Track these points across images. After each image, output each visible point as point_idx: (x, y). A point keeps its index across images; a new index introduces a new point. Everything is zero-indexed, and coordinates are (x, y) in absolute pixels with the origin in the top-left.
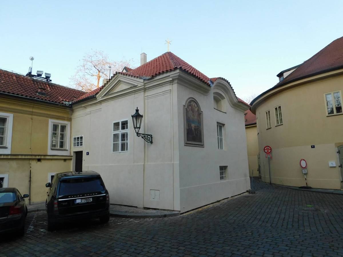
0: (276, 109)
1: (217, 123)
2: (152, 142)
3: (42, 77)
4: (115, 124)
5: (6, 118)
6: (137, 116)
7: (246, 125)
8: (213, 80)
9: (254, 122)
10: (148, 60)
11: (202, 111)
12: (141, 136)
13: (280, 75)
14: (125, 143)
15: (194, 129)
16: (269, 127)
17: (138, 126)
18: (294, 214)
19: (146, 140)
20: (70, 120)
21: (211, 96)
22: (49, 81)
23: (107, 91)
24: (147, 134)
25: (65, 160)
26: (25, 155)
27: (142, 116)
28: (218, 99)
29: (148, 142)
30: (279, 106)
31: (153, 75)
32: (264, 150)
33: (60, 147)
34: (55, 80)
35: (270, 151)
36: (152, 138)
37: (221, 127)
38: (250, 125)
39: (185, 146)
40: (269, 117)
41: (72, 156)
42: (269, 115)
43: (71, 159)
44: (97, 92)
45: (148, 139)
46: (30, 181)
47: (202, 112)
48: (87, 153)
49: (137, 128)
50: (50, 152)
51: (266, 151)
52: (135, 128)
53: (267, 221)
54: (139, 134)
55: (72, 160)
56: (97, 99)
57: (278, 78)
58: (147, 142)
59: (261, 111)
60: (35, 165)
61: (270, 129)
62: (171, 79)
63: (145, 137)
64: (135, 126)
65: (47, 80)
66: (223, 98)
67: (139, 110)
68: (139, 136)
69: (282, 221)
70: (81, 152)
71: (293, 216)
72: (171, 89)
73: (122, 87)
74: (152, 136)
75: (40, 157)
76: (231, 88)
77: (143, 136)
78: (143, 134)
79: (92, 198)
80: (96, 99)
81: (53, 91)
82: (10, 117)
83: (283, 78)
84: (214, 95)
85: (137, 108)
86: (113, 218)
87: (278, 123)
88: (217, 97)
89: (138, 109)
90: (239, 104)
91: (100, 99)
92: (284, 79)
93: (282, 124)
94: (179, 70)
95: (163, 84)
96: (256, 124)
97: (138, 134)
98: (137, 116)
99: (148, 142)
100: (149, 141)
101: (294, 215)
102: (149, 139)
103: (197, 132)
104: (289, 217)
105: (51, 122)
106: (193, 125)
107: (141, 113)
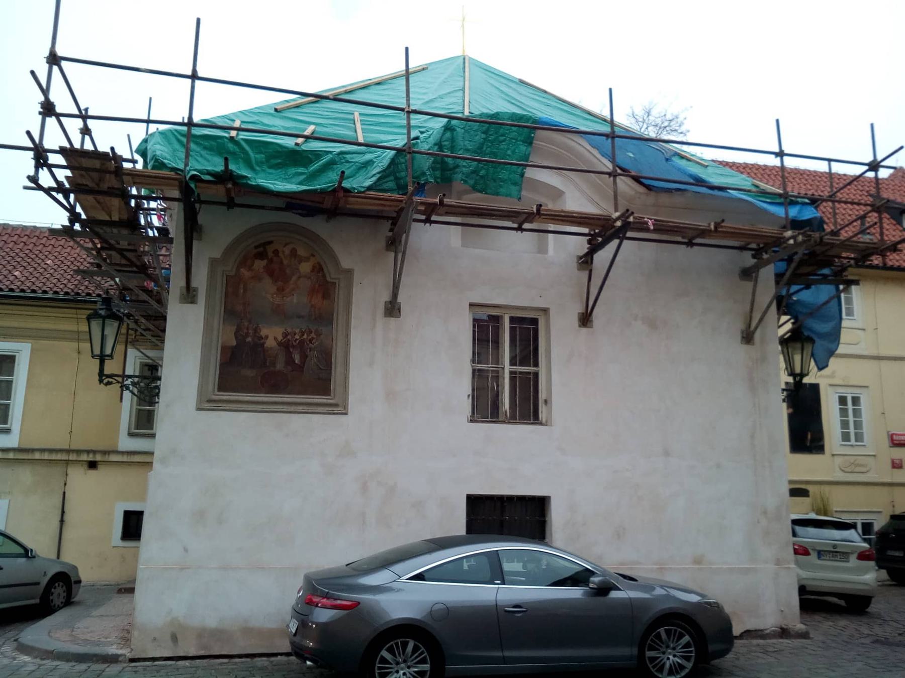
5: (15, 356)
12: (118, 382)
23: (372, 127)
26: (51, 451)
33: (856, 441)
46: (62, 521)
60: (79, 478)
75: (91, 455)
82: (23, 351)
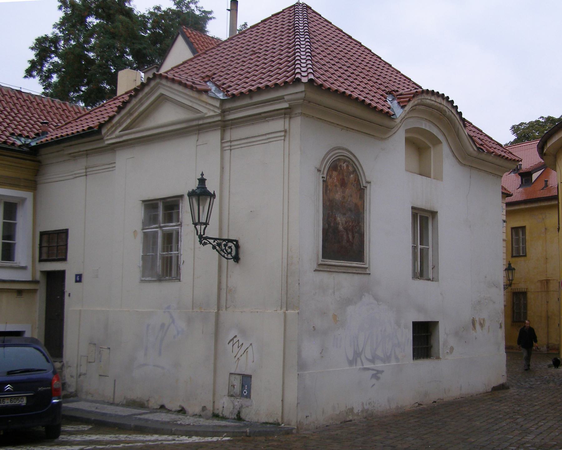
2: (237, 259)
4: (150, 205)
6: (201, 193)
11: (368, 180)
12: (210, 243)
14: (173, 255)
15: (344, 228)
17: (203, 220)
19: (223, 254)
20: (32, 185)
21: (399, 139)
24: (226, 238)
25: (20, 292)
27: (213, 196)
28: (419, 146)
36: (237, 247)
37: (427, 218)
39: (315, 271)
43: (35, 291)
45: (230, 250)
47: (369, 183)
48: (76, 275)
49: (202, 224)
52: (195, 224)
54: (206, 238)
55: (38, 292)
56: (105, 138)
61: (367, 276)
62: (286, 105)
63: (219, 245)
64: (197, 221)
66: (436, 142)
67: (206, 180)
68: (205, 244)
70: (61, 274)
72: (287, 127)
73: (167, 116)
77: (215, 243)
78: (215, 239)
79: (163, 202)
80: (102, 139)
84: (409, 135)
85: (202, 175)
89: (204, 177)
91: (111, 139)
95: (268, 114)
97: (203, 239)
98: (201, 193)
100: (229, 256)
102: (229, 250)
103: (350, 237)
106: (341, 219)
107: (211, 187)
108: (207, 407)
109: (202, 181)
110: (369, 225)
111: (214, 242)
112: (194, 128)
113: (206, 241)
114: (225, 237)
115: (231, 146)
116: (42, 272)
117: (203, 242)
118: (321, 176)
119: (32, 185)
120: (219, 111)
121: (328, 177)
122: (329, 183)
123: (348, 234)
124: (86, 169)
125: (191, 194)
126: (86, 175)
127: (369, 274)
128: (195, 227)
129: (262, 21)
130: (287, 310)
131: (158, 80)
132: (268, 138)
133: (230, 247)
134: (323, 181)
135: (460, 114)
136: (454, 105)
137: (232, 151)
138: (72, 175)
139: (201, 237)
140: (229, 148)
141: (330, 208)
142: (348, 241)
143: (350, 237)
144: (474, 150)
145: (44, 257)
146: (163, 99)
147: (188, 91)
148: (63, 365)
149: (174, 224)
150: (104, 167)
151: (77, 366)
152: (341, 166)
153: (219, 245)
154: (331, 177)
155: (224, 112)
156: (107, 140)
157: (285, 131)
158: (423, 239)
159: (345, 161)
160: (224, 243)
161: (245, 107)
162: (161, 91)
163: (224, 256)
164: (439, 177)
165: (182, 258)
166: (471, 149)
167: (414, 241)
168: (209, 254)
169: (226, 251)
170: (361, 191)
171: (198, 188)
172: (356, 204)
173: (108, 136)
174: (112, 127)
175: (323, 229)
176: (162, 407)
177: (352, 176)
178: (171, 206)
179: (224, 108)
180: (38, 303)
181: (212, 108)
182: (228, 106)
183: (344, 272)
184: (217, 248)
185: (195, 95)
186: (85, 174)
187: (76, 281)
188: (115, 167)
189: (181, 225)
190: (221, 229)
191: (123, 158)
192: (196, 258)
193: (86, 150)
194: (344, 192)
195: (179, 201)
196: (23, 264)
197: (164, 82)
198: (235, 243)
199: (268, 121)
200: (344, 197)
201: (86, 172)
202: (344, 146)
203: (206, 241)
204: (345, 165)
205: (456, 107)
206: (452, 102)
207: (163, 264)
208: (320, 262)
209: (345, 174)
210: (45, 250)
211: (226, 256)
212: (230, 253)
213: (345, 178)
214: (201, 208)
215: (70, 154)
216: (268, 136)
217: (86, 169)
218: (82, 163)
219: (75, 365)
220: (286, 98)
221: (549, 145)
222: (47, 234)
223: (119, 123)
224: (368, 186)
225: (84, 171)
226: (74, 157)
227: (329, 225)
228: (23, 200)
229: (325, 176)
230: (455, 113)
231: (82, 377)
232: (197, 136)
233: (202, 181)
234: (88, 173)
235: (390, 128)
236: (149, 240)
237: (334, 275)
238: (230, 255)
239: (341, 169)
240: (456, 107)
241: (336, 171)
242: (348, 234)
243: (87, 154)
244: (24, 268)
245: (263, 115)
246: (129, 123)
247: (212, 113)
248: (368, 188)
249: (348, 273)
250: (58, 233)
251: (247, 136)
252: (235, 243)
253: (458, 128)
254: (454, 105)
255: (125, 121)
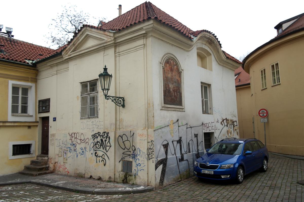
0: (273, 66)
1: (202, 83)
2: (123, 106)
3: (2, 31)
4: (84, 85)
7: (236, 87)
8: (196, 34)
9: (247, 83)
10: (124, 11)
11: (182, 69)
12: (111, 99)
13: (278, 27)
15: (173, 90)
16: (265, 88)
17: (106, 87)
18: (291, 189)
19: (117, 104)
22: (11, 37)
25: (29, 127)
29: (119, 106)
30: (276, 63)
31: (124, 27)
32: (259, 113)
34: (18, 36)
35: (265, 114)
36: (124, 100)
37: (206, 87)
38: (242, 87)
39: (161, 110)
40: (265, 77)
41: (38, 122)
42: (265, 74)
43: (37, 126)
44: (63, 49)
45: (120, 102)
47: (183, 70)
48: (54, 118)
50: (11, 118)
51: (261, 115)
52: (103, 90)
53: (257, 198)
54: (108, 96)
55: (38, 126)
56: (63, 57)
57: (276, 30)
58: (119, 107)
59: (256, 70)
61: (266, 90)
62: (144, 32)
64: (104, 88)
65: (9, 36)
68: (108, 99)
69: (276, 198)
70: (47, 118)
71: (290, 192)
72: (145, 43)
73: (91, 43)
74: (123, 98)
76: (218, 43)
77: (113, 99)
78: (113, 97)
81: (12, 47)
83: (282, 30)
84: (199, 51)
85: (105, 66)
86: (76, 195)
87: (275, 83)
88: (202, 53)
89: (106, 67)
90: (228, 61)
92: (283, 31)
93: (280, 84)
94: (153, 21)
95: (136, 37)
96: (249, 84)
97: (106, 97)
98: (105, 75)
99: (119, 106)
100: (120, 105)
101: (290, 191)
102: (120, 102)
103: (176, 94)
104: (285, 193)
105: (11, 83)
106: (171, 86)
107: (109, 72)
108: (112, 177)
109: (105, 69)
110: (184, 89)
111: (113, 98)
112: (103, 48)
113: (108, 98)
114: (118, 96)
115: (119, 55)
116: (40, 118)
117: (107, 98)
118: (162, 65)
119: (35, 80)
120: (113, 38)
121: (165, 67)
122: (165, 69)
123: (174, 93)
124: (57, 71)
125: (100, 75)
126: (57, 74)
127: (185, 111)
128: (103, 91)
129: (132, 10)
130: (148, 129)
131: (85, 28)
132: (136, 49)
133: (120, 101)
134: (163, 68)
135: (219, 42)
136: (217, 38)
137: (120, 57)
138: (51, 75)
139: (106, 96)
140: (118, 56)
141: (166, 81)
142: (175, 96)
143: (176, 94)
144: (225, 58)
145: (41, 111)
146: (88, 37)
147: (99, 31)
148: (48, 158)
149: (95, 92)
150: (64, 70)
151: (54, 158)
152: (170, 62)
153: (115, 100)
154: (166, 66)
155: (115, 39)
156: (65, 57)
157: (144, 45)
158: (206, 97)
159: (172, 60)
160: (117, 99)
161: (125, 35)
162: (87, 33)
163: (118, 105)
164: (211, 70)
165: (99, 107)
166: (224, 58)
167: (202, 98)
168: (110, 104)
169: (118, 102)
170: (179, 73)
171: (103, 73)
172: (177, 80)
173: (65, 56)
174: (67, 51)
175: (164, 90)
176: (91, 177)
177: (175, 67)
178: (93, 84)
179: (115, 37)
180: (37, 132)
181: (110, 38)
182: (117, 35)
183: (174, 111)
184: (114, 101)
185: (102, 32)
186: (56, 74)
187: (54, 121)
188: (68, 69)
189: (98, 92)
190: (116, 92)
191: (72, 65)
192: (105, 106)
193: (57, 63)
194: (172, 74)
195: (96, 81)
196: (31, 114)
197: (88, 28)
198: (122, 99)
199: (136, 41)
200: (172, 76)
201: (57, 73)
202: (171, 53)
203: (108, 98)
204: (172, 61)
205: (217, 39)
206: (216, 36)
207: (90, 110)
208: (163, 106)
209: (172, 65)
210: (41, 108)
211: (118, 105)
212: (121, 103)
213: (173, 67)
214: (105, 82)
215: (50, 65)
216: (136, 48)
217: (57, 71)
218: (55, 69)
219: (53, 158)
220: (144, 28)
221: (246, 62)
222: (41, 101)
223: (70, 49)
224: (182, 71)
225: (56, 72)
226: (52, 66)
227: (166, 89)
228: (31, 87)
229: (163, 66)
230: (217, 41)
231: (56, 163)
232: (103, 52)
233: (105, 69)
234: (58, 73)
235: (191, 46)
236: (84, 99)
237: (170, 112)
238: (120, 104)
239: (170, 63)
240: (217, 39)
241: (168, 64)
242: (174, 93)
243: (57, 64)
244: (32, 116)
245: (133, 38)
246: (74, 49)
247: (110, 40)
248: (182, 72)
249: (175, 111)
250: (46, 100)
251: (127, 49)
252: (122, 99)
253: (218, 48)
254: (217, 38)
255: (72, 48)
